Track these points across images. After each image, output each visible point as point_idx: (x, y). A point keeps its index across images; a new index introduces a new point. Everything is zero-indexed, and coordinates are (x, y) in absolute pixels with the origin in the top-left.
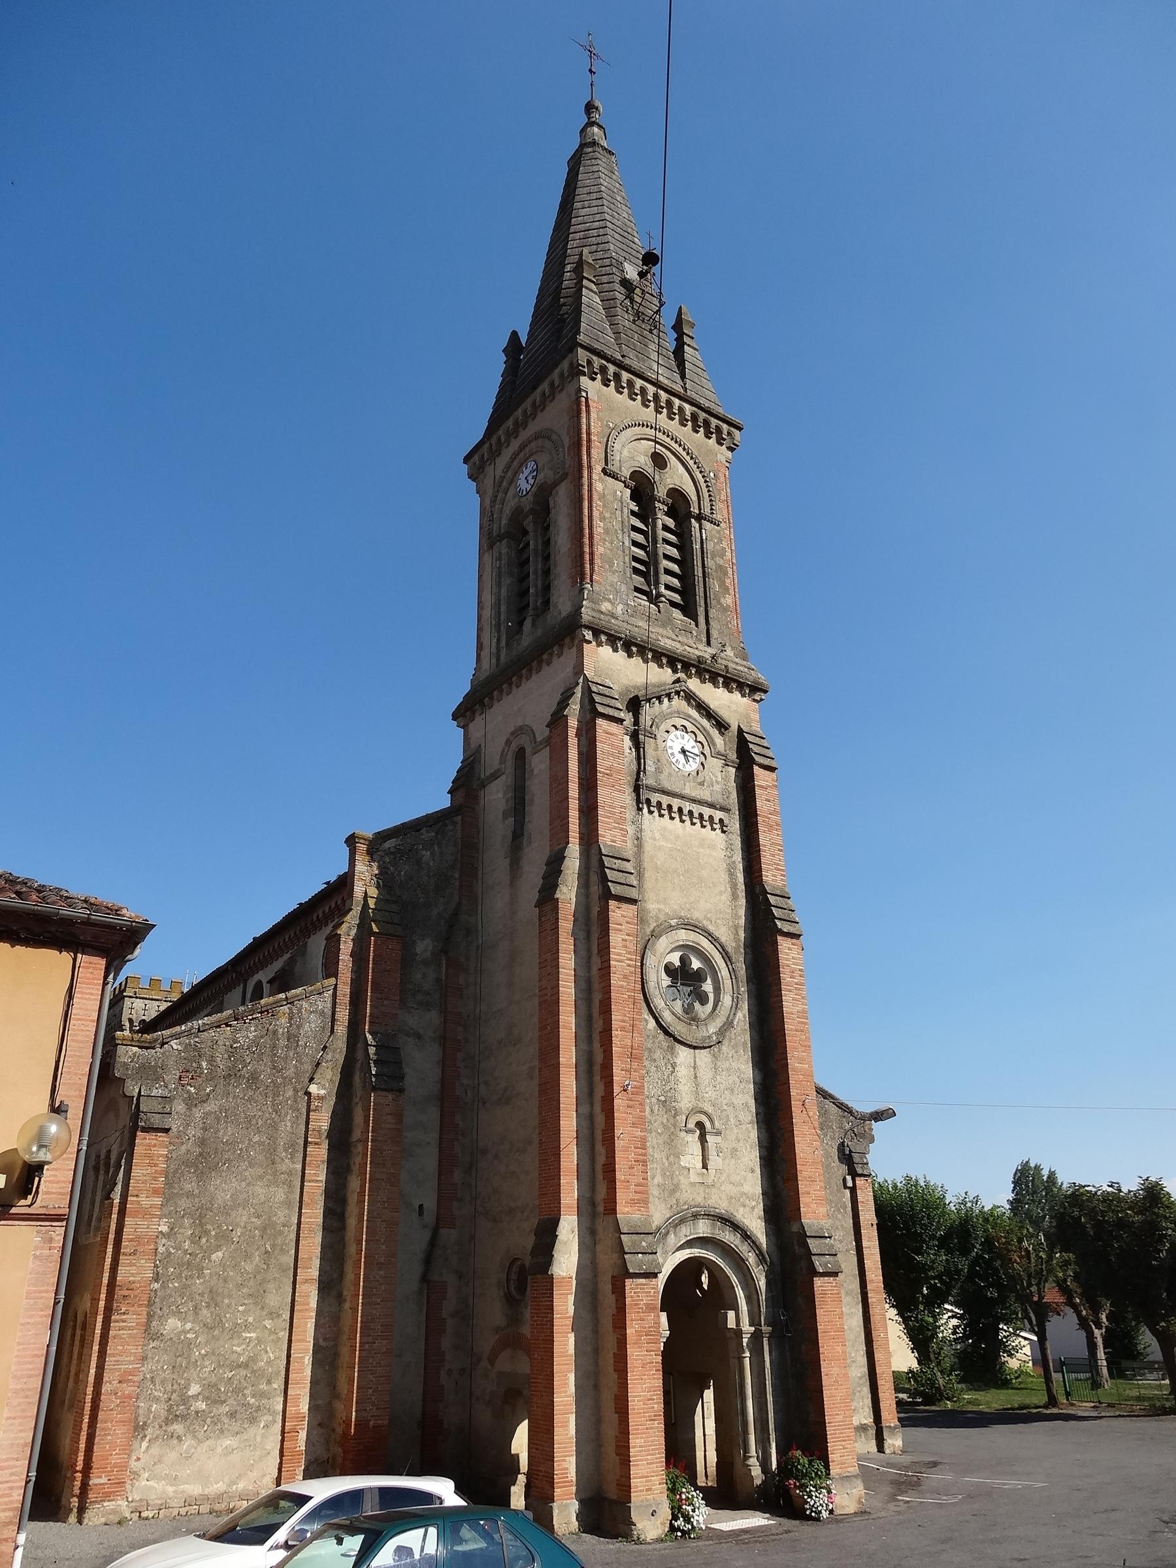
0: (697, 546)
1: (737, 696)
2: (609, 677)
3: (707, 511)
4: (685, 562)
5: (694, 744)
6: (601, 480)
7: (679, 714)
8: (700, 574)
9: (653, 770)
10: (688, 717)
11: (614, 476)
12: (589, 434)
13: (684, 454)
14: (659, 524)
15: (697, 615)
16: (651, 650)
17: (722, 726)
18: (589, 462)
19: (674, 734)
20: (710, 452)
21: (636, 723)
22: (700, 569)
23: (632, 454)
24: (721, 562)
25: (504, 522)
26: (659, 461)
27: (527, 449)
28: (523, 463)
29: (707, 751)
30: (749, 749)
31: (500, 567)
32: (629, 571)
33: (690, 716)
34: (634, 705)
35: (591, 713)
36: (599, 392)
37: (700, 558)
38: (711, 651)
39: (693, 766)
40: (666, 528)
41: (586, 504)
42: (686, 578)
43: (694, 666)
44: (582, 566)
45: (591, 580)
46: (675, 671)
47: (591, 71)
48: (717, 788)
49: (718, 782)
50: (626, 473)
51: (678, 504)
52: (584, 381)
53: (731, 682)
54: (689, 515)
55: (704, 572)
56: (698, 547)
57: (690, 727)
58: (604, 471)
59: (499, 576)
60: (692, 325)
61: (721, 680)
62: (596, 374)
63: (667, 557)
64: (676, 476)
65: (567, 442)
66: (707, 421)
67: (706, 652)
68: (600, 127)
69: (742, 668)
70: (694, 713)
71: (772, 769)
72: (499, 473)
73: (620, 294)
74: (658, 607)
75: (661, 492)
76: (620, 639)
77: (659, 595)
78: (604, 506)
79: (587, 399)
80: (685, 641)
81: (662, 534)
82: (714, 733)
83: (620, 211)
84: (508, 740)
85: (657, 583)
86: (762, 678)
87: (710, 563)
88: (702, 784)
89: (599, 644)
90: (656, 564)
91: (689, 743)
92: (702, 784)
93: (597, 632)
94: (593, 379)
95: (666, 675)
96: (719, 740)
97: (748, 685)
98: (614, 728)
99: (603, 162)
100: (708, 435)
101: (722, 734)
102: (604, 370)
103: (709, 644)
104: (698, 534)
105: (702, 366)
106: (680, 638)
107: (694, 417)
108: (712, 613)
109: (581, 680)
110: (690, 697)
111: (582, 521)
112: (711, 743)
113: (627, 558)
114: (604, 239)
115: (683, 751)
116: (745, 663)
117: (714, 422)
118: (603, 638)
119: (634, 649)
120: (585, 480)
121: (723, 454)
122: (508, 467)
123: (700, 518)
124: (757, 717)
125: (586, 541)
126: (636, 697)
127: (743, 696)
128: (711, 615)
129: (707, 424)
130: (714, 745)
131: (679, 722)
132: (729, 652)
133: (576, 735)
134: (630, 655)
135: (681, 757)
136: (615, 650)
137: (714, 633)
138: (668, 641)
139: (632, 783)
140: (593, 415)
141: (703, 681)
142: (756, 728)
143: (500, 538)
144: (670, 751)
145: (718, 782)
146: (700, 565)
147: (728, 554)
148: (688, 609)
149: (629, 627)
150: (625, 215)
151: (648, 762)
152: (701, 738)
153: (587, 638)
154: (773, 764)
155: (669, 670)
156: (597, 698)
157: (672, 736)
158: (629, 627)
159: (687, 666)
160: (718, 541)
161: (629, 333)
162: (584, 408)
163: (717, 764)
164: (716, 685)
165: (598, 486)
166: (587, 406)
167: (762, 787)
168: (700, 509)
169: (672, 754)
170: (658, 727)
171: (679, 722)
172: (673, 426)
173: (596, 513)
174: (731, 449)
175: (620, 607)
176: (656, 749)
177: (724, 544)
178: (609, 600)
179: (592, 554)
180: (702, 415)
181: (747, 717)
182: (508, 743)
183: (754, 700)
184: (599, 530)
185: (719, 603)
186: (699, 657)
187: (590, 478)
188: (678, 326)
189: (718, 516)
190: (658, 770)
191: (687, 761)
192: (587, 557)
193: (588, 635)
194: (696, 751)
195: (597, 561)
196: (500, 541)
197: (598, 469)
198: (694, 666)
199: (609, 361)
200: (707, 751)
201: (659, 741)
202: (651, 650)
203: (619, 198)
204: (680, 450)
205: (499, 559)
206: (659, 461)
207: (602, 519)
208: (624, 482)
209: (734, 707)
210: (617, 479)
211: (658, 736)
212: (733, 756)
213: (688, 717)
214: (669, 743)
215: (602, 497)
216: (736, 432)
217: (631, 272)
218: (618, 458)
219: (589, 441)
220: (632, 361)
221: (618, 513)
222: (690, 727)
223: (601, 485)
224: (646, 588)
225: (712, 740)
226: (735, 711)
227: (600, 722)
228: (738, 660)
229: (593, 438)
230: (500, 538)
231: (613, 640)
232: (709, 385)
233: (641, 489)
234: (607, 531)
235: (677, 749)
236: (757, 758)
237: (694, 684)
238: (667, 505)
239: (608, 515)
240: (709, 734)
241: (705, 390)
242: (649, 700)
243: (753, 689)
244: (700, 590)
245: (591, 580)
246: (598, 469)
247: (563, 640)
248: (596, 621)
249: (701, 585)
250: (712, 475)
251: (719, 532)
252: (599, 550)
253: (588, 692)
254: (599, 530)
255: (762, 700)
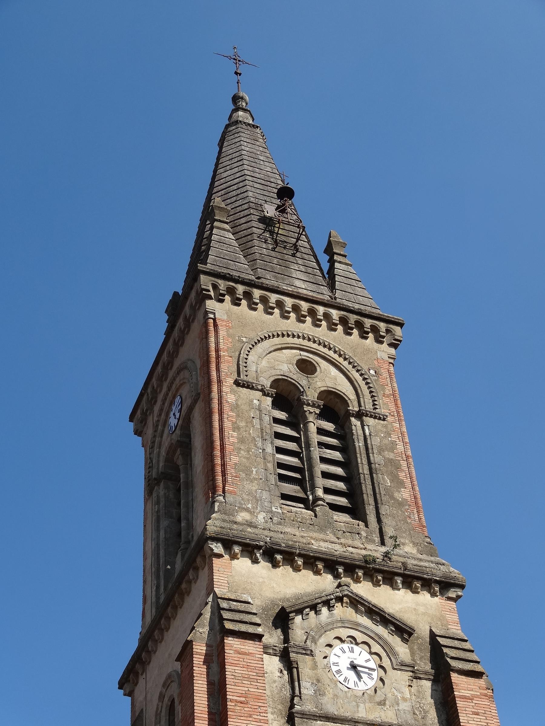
0: (360, 444)
1: (425, 597)
2: (245, 591)
3: (368, 406)
4: (349, 464)
5: (368, 656)
6: (232, 391)
7: (343, 623)
8: (366, 471)
9: (311, 692)
10: (356, 626)
11: (249, 386)
12: (217, 350)
13: (336, 356)
14: (312, 428)
15: (365, 514)
16: (300, 555)
17: (404, 631)
18: (219, 376)
19: (338, 647)
20: (369, 350)
21: (286, 640)
22: (366, 467)
23: (273, 363)
24: (391, 456)
25: (161, 464)
26: (306, 367)
27: (174, 386)
28: (172, 403)
29: (386, 662)
30: (443, 655)
31: (158, 512)
32: (273, 479)
33: (358, 624)
34: (282, 619)
35: (220, 632)
36: (228, 313)
37: (364, 455)
38: (383, 549)
39: (369, 683)
40: (321, 431)
41: (216, 417)
42: (351, 479)
43: (360, 567)
44: (214, 480)
45: (224, 492)
46: (337, 576)
47: (236, 73)
48: (404, 706)
49: (404, 699)
50: (267, 384)
51: (333, 407)
52: (210, 304)
53: (413, 580)
54: (348, 414)
55: (370, 469)
56: (362, 444)
57: (361, 638)
58: (237, 383)
59: (158, 520)
60: (344, 245)
61: (399, 580)
62: (224, 295)
63: (324, 460)
64: (328, 378)
65: (198, 364)
66: (356, 321)
67: (376, 551)
68: (245, 110)
69: (426, 564)
70: (365, 621)
71: (478, 675)
72: (156, 419)
73: (257, 228)
74: (314, 511)
75: (311, 395)
76: (259, 547)
77: (317, 499)
78: (238, 416)
79: (214, 320)
80: (350, 542)
81: (315, 438)
82: (395, 641)
83: (262, 167)
84: (161, 693)
85: (313, 488)
86: (455, 572)
87: (376, 458)
88: (382, 703)
89: (234, 557)
90: (311, 468)
91: (361, 656)
92: (382, 703)
93: (228, 544)
94: (222, 301)
95: (326, 583)
96: (402, 650)
97: (436, 582)
98: (250, 646)
99: (245, 135)
100: (363, 335)
101: (405, 641)
102: (231, 291)
103: (383, 543)
104: (360, 432)
105: (357, 277)
106: (342, 541)
107: (343, 321)
108: (383, 510)
109: (210, 599)
110: (356, 602)
111: (211, 434)
112: (390, 652)
113: (270, 466)
114: (244, 189)
115: (354, 667)
116: (432, 559)
117: (368, 323)
118: (237, 549)
119: (279, 557)
120: (215, 394)
121: (385, 351)
122: (161, 410)
123: (360, 415)
124: (455, 617)
125: (217, 453)
126: (283, 609)
127: (433, 595)
128: (382, 511)
129: (359, 325)
130: (395, 654)
131: (344, 633)
132: (409, 549)
133: (205, 662)
134: (275, 565)
135: (351, 675)
136: (255, 561)
137: (389, 531)
138: (323, 544)
139: (285, 712)
140: (222, 332)
141: (376, 584)
142: (456, 630)
143: (157, 481)
144: (334, 669)
145: (404, 699)
146: (365, 461)
147: (400, 447)
148: (356, 511)
149: (272, 534)
150: (269, 169)
151: (303, 684)
152: (376, 648)
153: (216, 551)
154: (478, 668)
155: (330, 577)
156: (226, 615)
157: (336, 650)
158: (272, 534)
159: (351, 568)
160: (386, 437)
161: (267, 259)
162: (212, 328)
163: (402, 678)
164: (394, 586)
165: (230, 398)
166: (215, 325)
167: (464, 697)
168: (360, 405)
169: (339, 672)
170: (314, 641)
171: (344, 633)
172: (322, 332)
173: (227, 424)
174: (391, 345)
175: (261, 517)
176: (315, 667)
177: (394, 437)
178: (247, 510)
179: (223, 465)
180: (353, 318)
181: (442, 618)
182: (161, 697)
183: (449, 599)
184: (231, 440)
185: (392, 497)
186: (365, 556)
187: (220, 391)
188: (329, 250)
189: (382, 410)
190: (319, 693)
191: (359, 677)
192: (219, 469)
193: (217, 548)
194: (372, 664)
195: (230, 471)
196: (158, 484)
197: (228, 382)
198: (360, 567)
199: (237, 281)
200: (386, 662)
201: (319, 657)
202: (300, 555)
203: (262, 158)
204: (331, 353)
205: (158, 503)
206: (306, 367)
207: (236, 428)
208: (262, 390)
209: (422, 609)
210: (252, 388)
211: (317, 652)
212: (426, 666)
213: (356, 626)
214: (333, 659)
215: (235, 407)
216: (397, 330)
217: (270, 211)
218: (254, 369)
219: (218, 357)
220: (270, 280)
221: (256, 422)
222: (361, 638)
223: (231, 395)
224: (302, 495)
225: (392, 649)
226: (424, 614)
227: (229, 641)
228: (424, 557)
229: (222, 353)
230: (157, 481)
231: (250, 550)
232: (366, 294)
233: (285, 396)
234: (242, 440)
235: (344, 664)
236: (454, 664)
237: (364, 589)
238: (318, 407)
239: (242, 424)
240: (386, 642)
241: (361, 297)
242: (300, 611)
243: (444, 586)
244: (367, 488)
245: (224, 492)
246: (228, 382)
247: (194, 561)
248: (224, 531)
249: (369, 482)
250: (372, 372)
251: (386, 427)
252: (233, 459)
253: (217, 610)
254: (231, 440)
255: (459, 597)
